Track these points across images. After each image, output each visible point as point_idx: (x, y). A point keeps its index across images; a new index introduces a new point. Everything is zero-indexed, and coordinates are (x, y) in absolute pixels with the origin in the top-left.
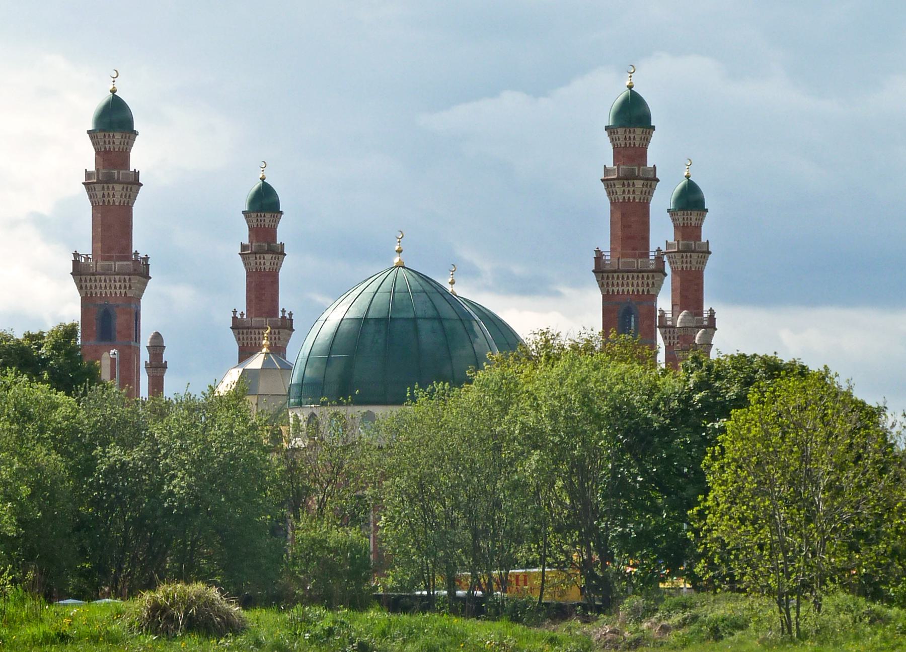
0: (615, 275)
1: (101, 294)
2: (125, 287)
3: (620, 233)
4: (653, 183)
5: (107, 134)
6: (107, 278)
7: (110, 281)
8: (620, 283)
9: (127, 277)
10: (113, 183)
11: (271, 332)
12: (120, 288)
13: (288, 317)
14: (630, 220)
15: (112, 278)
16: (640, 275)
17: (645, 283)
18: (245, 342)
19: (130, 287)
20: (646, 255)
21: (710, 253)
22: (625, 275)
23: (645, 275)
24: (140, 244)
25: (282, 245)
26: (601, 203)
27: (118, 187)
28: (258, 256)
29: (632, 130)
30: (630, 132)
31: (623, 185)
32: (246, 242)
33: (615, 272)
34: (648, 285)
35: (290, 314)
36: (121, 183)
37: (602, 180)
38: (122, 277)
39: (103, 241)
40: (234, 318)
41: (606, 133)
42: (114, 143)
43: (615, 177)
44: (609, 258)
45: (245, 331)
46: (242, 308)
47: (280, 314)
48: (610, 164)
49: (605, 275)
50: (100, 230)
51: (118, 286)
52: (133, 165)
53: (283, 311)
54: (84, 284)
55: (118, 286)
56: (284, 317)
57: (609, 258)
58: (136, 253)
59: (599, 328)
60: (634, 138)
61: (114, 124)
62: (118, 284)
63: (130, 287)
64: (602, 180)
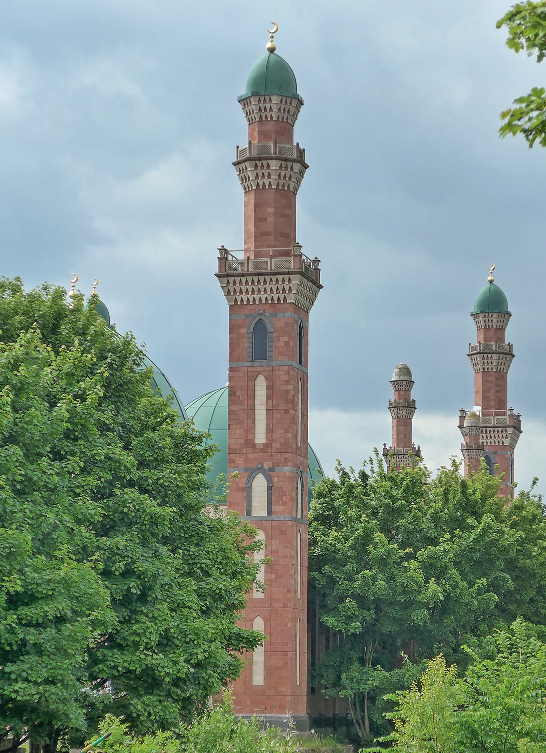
0: (244, 279)
8: (250, 290)
16: (274, 278)
22: (256, 279)
23: (280, 277)
31: (256, 166)
33: (243, 275)
36: (277, 159)
41: (240, 106)
49: (231, 280)
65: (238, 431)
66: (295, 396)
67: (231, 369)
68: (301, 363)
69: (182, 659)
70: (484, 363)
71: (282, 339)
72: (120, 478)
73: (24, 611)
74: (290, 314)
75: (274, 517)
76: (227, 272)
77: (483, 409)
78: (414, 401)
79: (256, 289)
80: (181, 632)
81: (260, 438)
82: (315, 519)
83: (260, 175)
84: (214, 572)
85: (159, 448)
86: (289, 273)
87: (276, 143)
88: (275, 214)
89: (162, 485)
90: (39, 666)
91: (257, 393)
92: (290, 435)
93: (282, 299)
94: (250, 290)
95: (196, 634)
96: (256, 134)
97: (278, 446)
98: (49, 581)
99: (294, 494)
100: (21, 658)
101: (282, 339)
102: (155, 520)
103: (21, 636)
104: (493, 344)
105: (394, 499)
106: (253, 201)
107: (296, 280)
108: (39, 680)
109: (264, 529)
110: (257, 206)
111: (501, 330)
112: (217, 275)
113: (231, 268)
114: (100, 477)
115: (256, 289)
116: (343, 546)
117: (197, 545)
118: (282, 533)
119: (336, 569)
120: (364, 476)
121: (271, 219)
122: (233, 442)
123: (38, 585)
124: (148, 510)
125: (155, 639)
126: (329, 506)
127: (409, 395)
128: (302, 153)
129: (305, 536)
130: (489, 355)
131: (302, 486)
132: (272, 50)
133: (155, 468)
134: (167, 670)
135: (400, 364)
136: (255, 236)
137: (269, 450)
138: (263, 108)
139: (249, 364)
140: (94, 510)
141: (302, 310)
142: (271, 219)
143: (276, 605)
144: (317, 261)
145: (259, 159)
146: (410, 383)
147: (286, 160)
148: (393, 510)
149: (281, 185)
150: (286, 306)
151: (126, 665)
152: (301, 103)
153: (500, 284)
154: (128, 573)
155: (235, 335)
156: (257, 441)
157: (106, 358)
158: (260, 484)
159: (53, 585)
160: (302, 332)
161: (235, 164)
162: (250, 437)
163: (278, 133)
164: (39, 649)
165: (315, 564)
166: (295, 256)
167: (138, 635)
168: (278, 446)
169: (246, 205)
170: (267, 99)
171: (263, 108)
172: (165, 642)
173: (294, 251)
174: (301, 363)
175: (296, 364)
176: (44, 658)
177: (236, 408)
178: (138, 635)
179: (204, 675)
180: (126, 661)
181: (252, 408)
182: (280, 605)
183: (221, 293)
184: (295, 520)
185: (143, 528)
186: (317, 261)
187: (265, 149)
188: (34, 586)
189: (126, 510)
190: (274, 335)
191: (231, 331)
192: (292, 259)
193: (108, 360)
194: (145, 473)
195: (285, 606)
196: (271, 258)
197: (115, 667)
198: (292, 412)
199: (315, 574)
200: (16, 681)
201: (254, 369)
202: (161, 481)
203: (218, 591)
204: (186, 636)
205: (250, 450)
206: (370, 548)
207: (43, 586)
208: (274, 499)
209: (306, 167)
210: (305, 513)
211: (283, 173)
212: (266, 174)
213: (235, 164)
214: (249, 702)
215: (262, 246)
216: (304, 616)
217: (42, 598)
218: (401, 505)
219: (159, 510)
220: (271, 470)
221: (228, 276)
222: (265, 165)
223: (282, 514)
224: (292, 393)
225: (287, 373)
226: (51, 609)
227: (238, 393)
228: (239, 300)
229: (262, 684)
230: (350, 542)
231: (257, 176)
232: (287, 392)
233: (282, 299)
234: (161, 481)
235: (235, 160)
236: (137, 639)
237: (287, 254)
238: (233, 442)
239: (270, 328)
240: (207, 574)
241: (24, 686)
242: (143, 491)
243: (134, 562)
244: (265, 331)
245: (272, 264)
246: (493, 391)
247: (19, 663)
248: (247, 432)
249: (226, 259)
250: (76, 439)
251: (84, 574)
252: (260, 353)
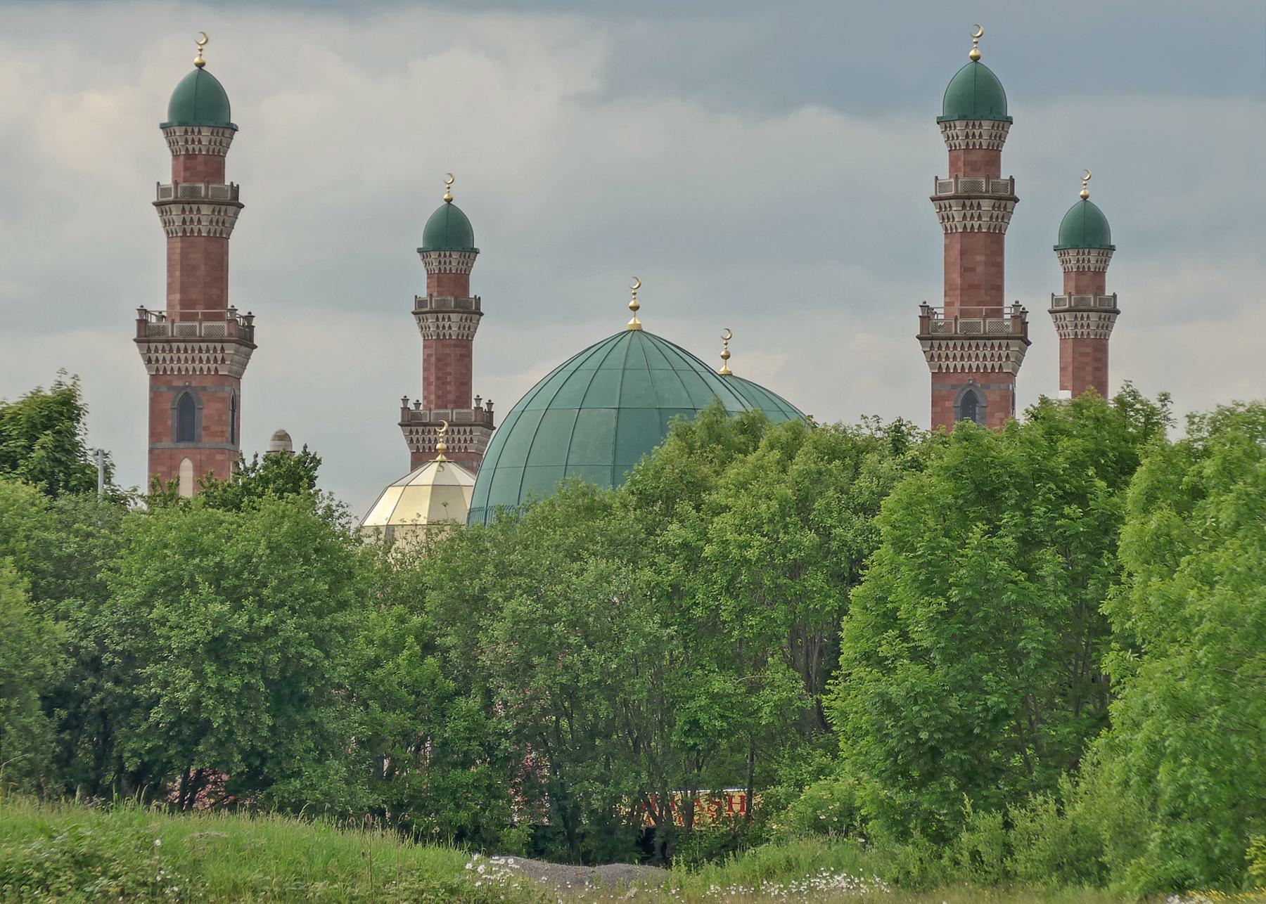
0: (951, 343)
1: (179, 369)
2: (216, 360)
3: (958, 281)
4: (1010, 203)
5: (189, 129)
6: (189, 346)
7: (193, 350)
8: (958, 356)
9: (219, 346)
10: (201, 202)
11: (447, 432)
12: (208, 361)
13: (485, 407)
14: (978, 264)
15: (196, 346)
16: (989, 343)
17: (996, 355)
18: (421, 445)
19: (223, 360)
20: (999, 313)
21: (1118, 312)
22: (966, 343)
23: (996, 343)
24: (239, 299)
25: (478, 300)
26: (930, 237)
27: (205, 210)
28: (440, 316)
29: (196, 130)
30: (974, 126)
31: (964, 206)
32: (423, 294)
33: (951, 339)
34: (1000, 357)
35: (490, 404)
36: (210, 203)
37: (156, 204)
38: (211, 345)
39: (183, 290)
40: (405, 409)
42: (200, 142)
43: (171, 199)
44: (942, 317)
45: (420, 429)
46: (416, 393)
47: (474, 405)
48: (945, 176)
49: (936, 343)
50: (178, 274)
51: (204, 359)
52: (231, 176)
53: (478, 399)
54: (153, 357)
55: (204, 359)
56: (478, 408)
57: (942, 317)
58: (234, 310)
59: (929, 428)
60: (980, 135)
61: (202, 114)
62: (204, 356)
63: (223, 360)
64: (933, 199)
68: (233, 442)
70: (1076, 326)
71: (997, 415)
76: (930, 335)
77: (1074, 396)
83: (969, 216)
93: (997, 367)
101: (997, 415)
104: (1091, 296)
106: (958, 246)
111: (1100, 274)
121: (980, 269)
130: (1085, 314)
136: (962, 290)
138: (970, 134)
145: (969, 198)
147: (1000, 199)
153: (1100, 202)
155: (939, 409)
170: (977, 123)
171: (970, 134)
174: (233, 442)
186: (249, 317)
187: (194, 191)
212: (976, 215)
221: (932, 339)
222: (975, 205)
231: (964, 217)
233: (997, 367)
237: (220, 317)
246: (1089, 369)
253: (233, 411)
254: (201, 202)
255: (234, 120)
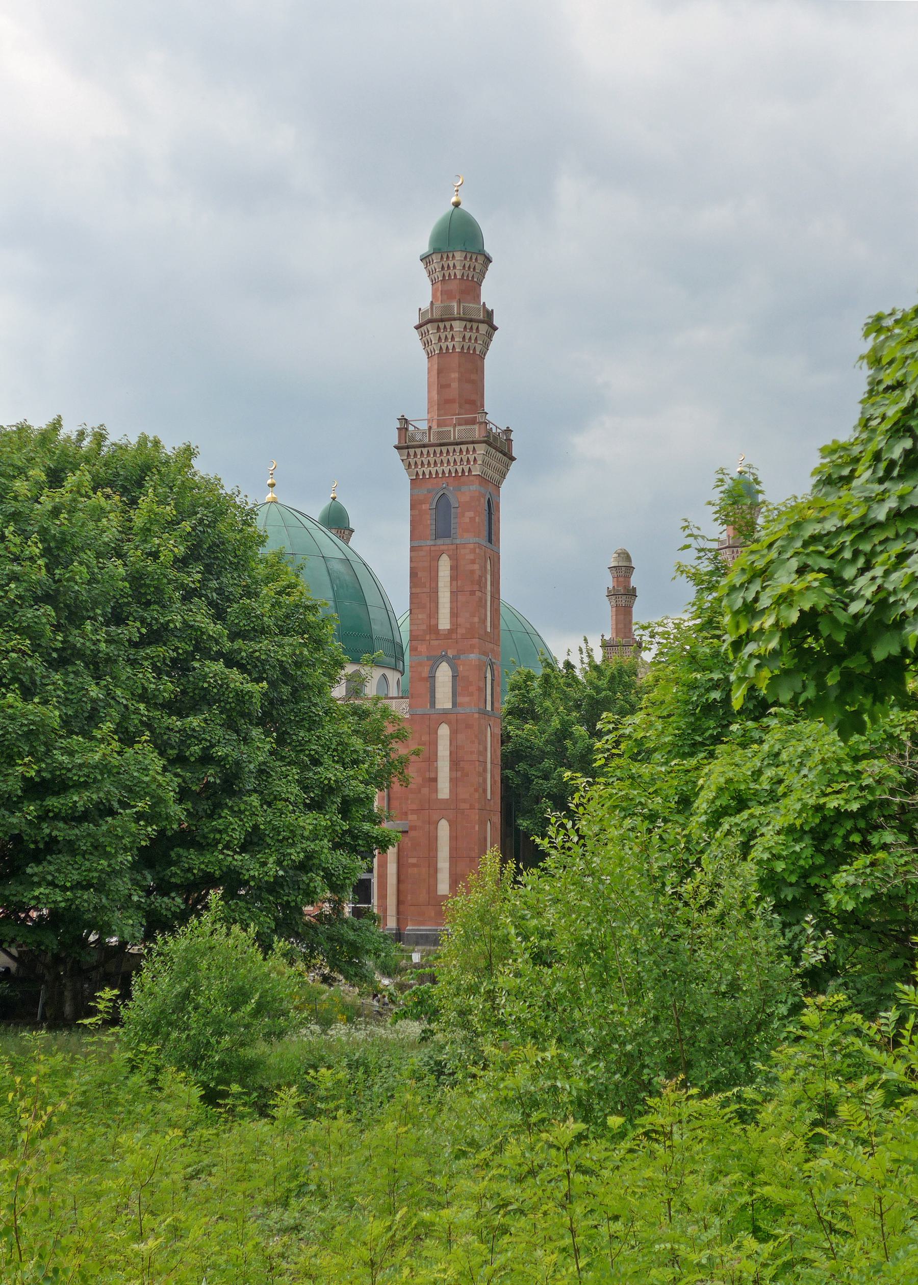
0: (425, 451)
8: (432, 462)
10: (459, 326)
16: (457, 448)
22: (438, 449)
23: (464, 447)
24: (498, 411)
33: (424, 446)
36: (460, 319)
41: (422, 265)
49: (412, 451)
65: (420, 616)
66: (482, 576)
67: (413, 549)
68: (490, 541)
69: (271, 860)
72: (201, 647)
73: (53, 802)
74: (475, 487)
75: (460, 710)
76: (407, 444)
78: (634, 589)
79: (438, 461)
80: (273, 829)
81: (444, 623)
82: (510, 713)
83: (443, 337)
84: (326, 759)
85: (257, 617)
86: (473, 442)
87: (459, 302)
88: (460, 380)
89: (258, 658)
90: (70, 867)
91: (441, 574)
92: (476, 620)
93: (466, 470)
94: (432, 462)
95: (292, 831)
96: (439, 294)
97: (464, 631)
98: (81, 766)
99: (482, 684)
100: (49, 858)
102: (241, 697)
103: (47, 831)
105: (598, 690)
106: (436, 367)
107: (481, 449)
108: (68, 884)
109: (449, 723)
110: (440, 372)
112: (397, 447)
113: (412, 438)
114: (178, 648)
115: (438, 461)
116: (539, 742)
117: (309, 730)
118: (468, 726)
119: (531, 766)
120: (569, 665)
122: (415, 628)
123: (69, 770)
124: (232, 686)
125: (238, 836)
126: (524, 698)
127: (629, 582)
128: (490, 314)
129: (498, 731)
131: (493, 675)
132: (457, 205)
133: (251, 640)
134: (252, 873)
135: (619, 547)
137: (454, 636)
139: (432, 543)
140: (168, 688)
141: (491, 486)
142: (455, 385)
143: (463, 806)
144: (508, 431)
145: (442, 320)
146: (630, 569)
147: (471, 320)
148: (598, 702)
149: (466, 348)
150: (472, 478)
151: (203, 866)
152: (488, 260)
154: (206, 759)
155: (417, 512)
156: (441, 627)
157: (197, 513)
158: (444, 673)
159: (86, 770)
160: (491, 510)
161: (417, 328)
162: (433, 622)
163: (462, 292)
164: (71, 848)
165: (509, 760)
166: (481, 423)
167: (220, 832)
168: (464, 631)
169: (430, 371)
170: (451, 255)
172: (253, 842)
173: (480, 418)
174: (490, 541)
175: (484, 542)
176: (78, 858)
177: (418, 590)
178: (220, 832)
179: (305, 878)
180: (203, 863)
181: (435, 591)
182: (467, 806)
183: (401, 466)
184: (483, 712)
185: (228, 706)
186: (508, 431)
187: (449, 309)
188: (64, 772)
189: (206, 685)
190: (459, 510)
191: (413, 507)
192: (476, 427)
193: (199, 516)
194: (239, 643)
195: (472, 807)
196: (455, 426)
197: (190, 870)
198: (478, 594)
199: (508, 772)
200: (39, 885)
201: (436, 548)
202: (257, 654)
203: (326, 782)
204: (279, 833)
205: (433, 636)
206: (568, 743)
207: (74, 771)
208: (459, 689)
209: (495, 329)
210: (496, 705)
211: (468, 335)
212: (449, 337)
213: (417, 328)
214: (433, 914)
215: (445, 414)
216: (497, 819)
217: (72, 787)
218: (606, 696)
219: (249, 687)
220: (454, 658)
221: (408, 447)
222: (448, 327)
223: (469, 707)
224: (478, 573)
225: (473, 551)
226: (79, 799)
227: (420, 574)
228: (421, 473)
229: (439, 893)
230: (545, 736)
232: (472, 572)
233: (466, 470)
234: (257, 654)
235: (417, 323)
236: (218, 836)
237: (473, 422)
238: (415, 628)
239: (454, 504)
240: (316, 762)
241: (47, 891)
242: (229, 664)
243: (212, 746)
244: (449, 505)
245: (456, 433)
247: (45, 863)
248: (430, 617)
249: (407, 429)
250: (148, 603)
251: (147, 762)
252: (443, 531)
253: (490, 513)
254: (459, 326)
255: (488, 249)
